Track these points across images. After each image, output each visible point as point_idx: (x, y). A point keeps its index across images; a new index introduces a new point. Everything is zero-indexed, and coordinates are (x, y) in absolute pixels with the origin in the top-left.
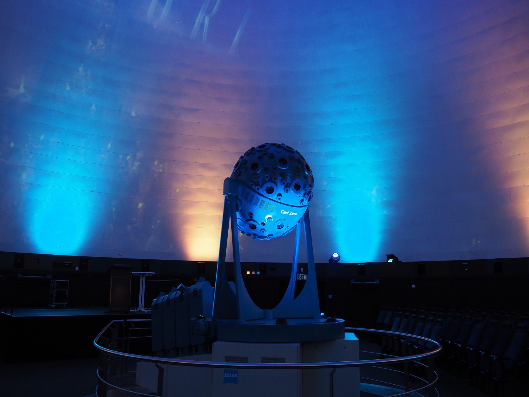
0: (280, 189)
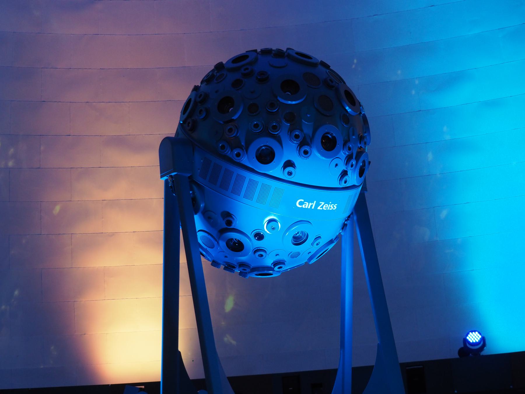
0: (289, 151)
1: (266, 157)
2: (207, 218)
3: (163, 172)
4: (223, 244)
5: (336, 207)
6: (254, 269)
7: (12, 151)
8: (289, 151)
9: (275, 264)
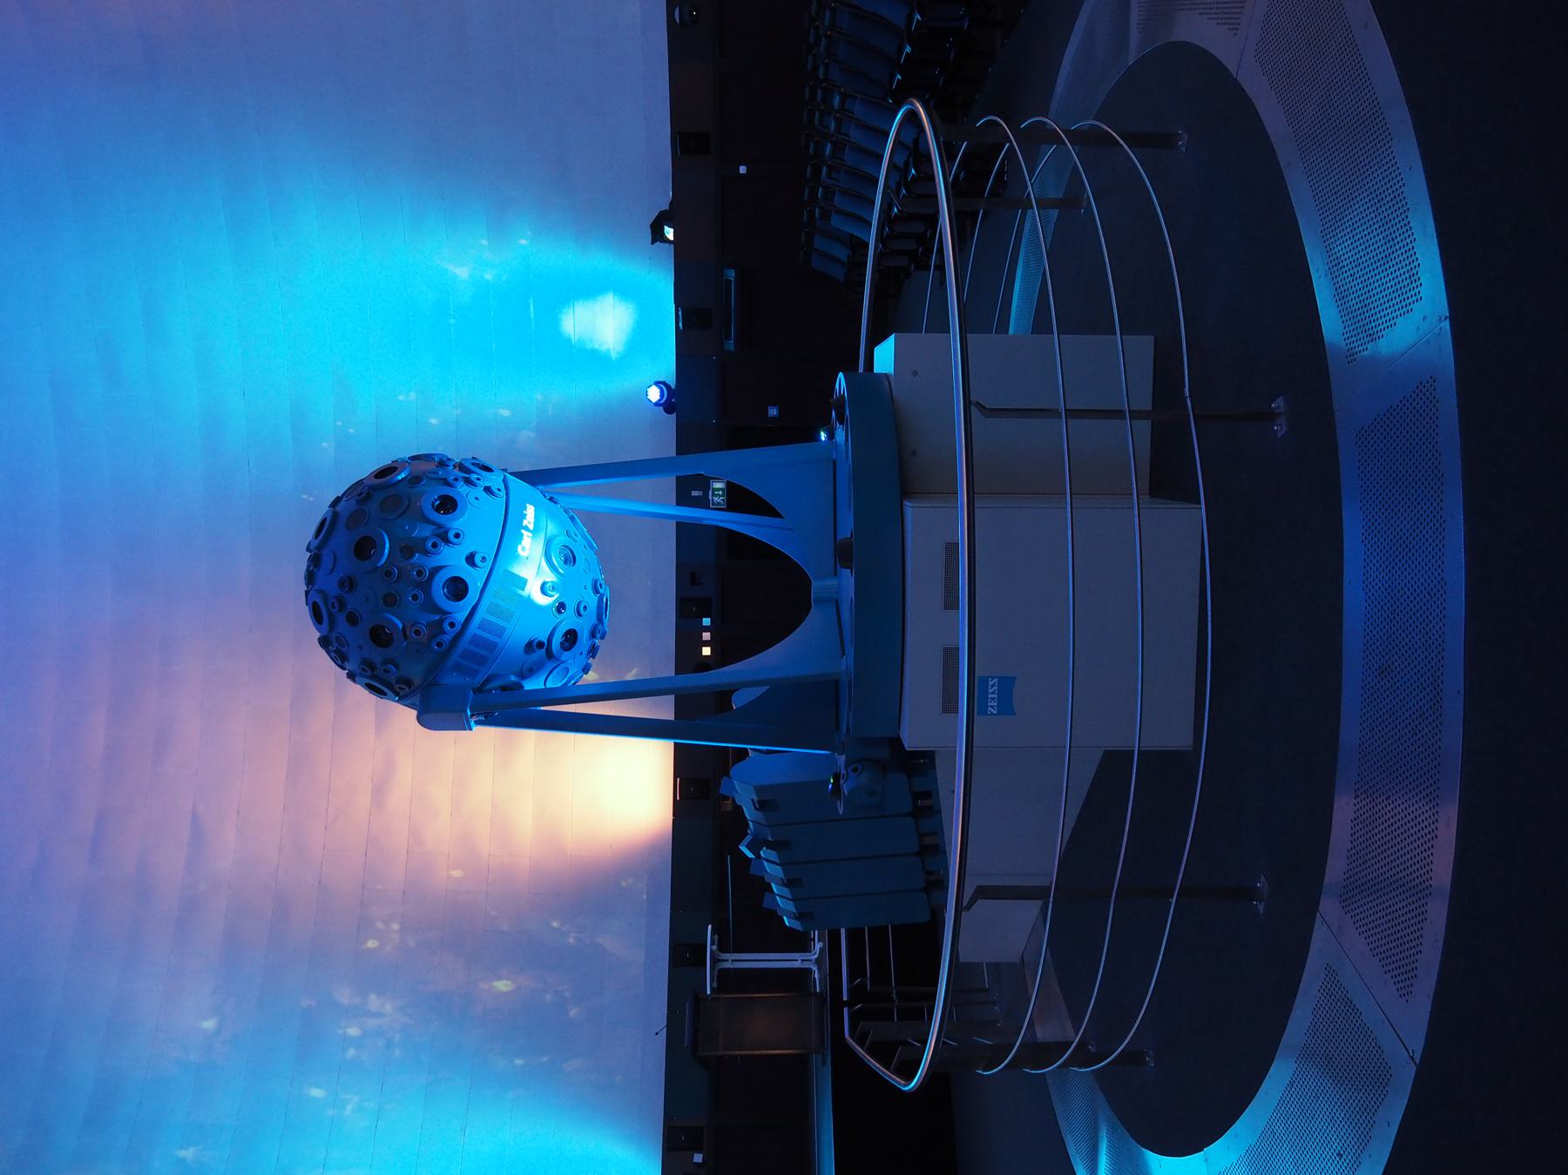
0: (452, 559)
1: (458, 588)
2: (530, 672)
3: (464, 726)
4: (566, 656)
6: (600, 619)
7: (379, 925)
8: (452, 559)
9: (596, 591)
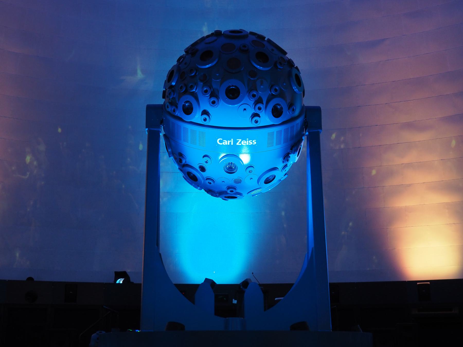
0: (205, 105)
5: (255, 143)
